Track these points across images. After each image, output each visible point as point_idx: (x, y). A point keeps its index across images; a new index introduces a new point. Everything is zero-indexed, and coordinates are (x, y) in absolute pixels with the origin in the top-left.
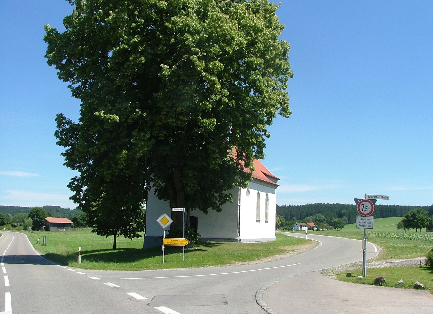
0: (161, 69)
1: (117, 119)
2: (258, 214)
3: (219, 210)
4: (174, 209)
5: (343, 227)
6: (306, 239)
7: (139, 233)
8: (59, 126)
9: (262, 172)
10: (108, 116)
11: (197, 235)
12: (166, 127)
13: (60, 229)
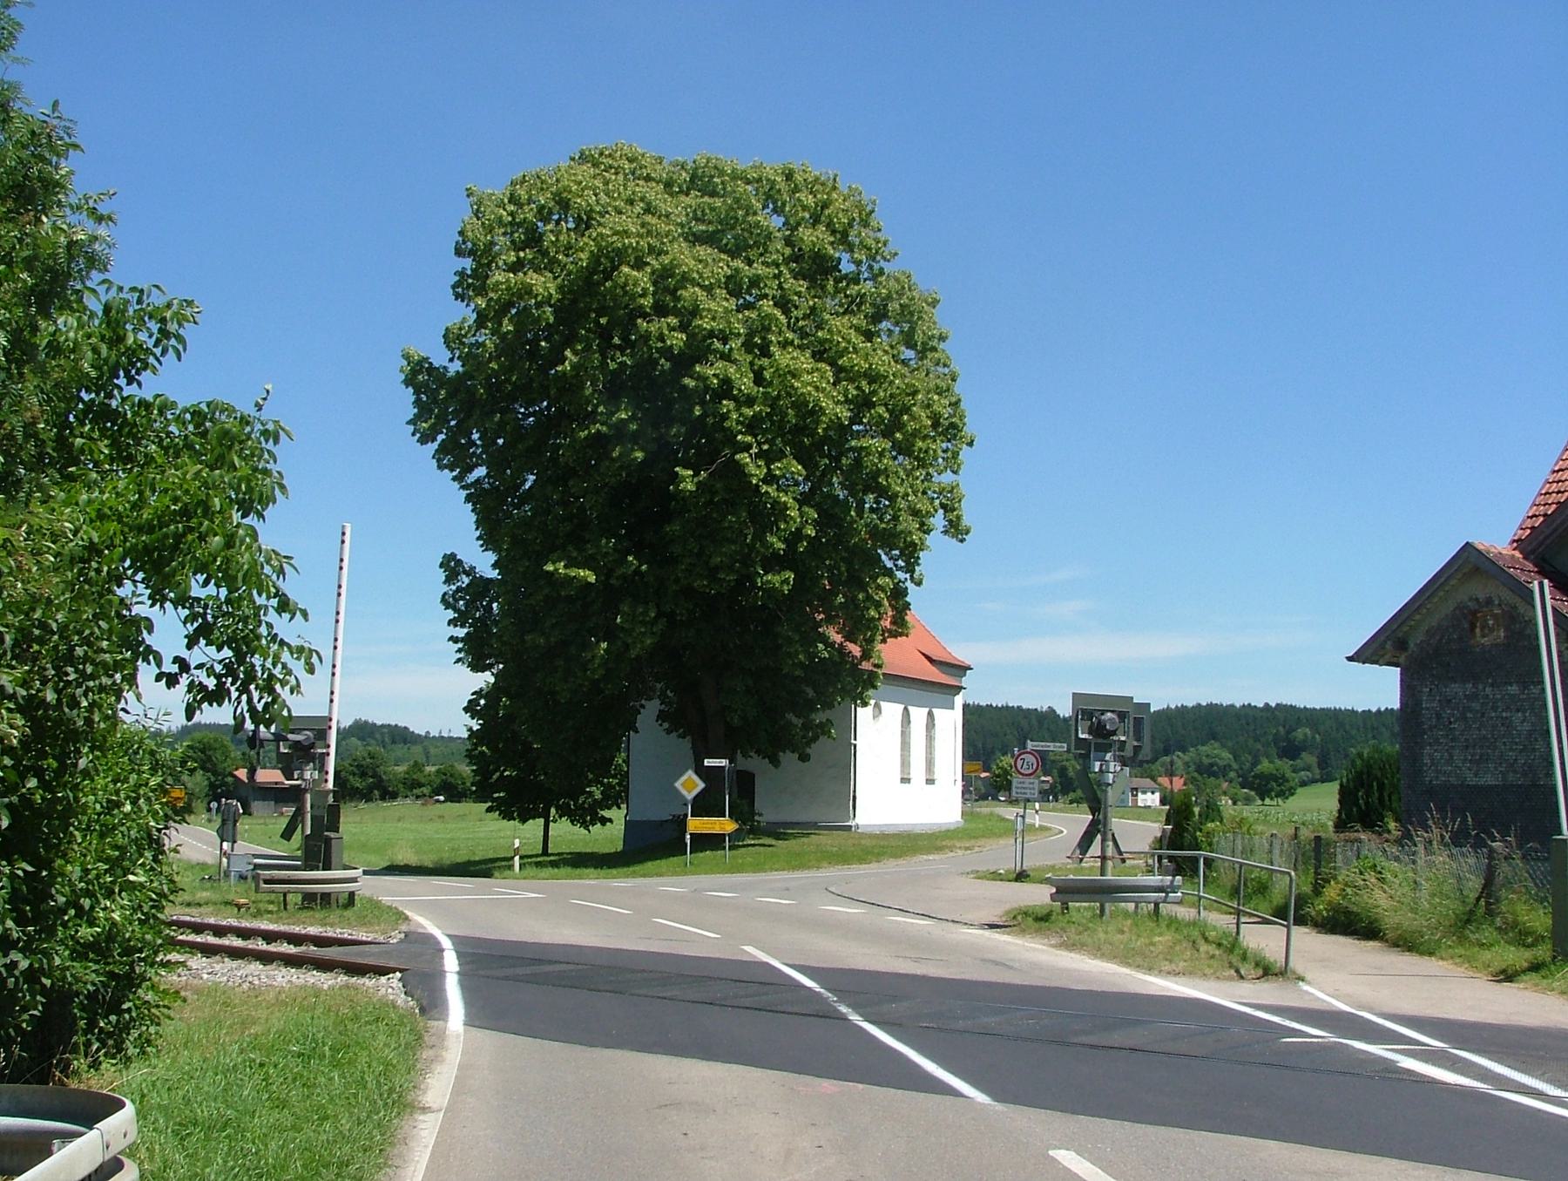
0: (675, 478)
1: (592, 579)
2: (905, 763)
3: (804, 758)
4: (707, 762)
5: (1292, 794)
6: (1037, 826)
7: (606, 813)
8: (448, 581)
9: (924, 654)
10: (573, 572)
11: (753, 813)
12: (688, 592)
13: (285, 809)
